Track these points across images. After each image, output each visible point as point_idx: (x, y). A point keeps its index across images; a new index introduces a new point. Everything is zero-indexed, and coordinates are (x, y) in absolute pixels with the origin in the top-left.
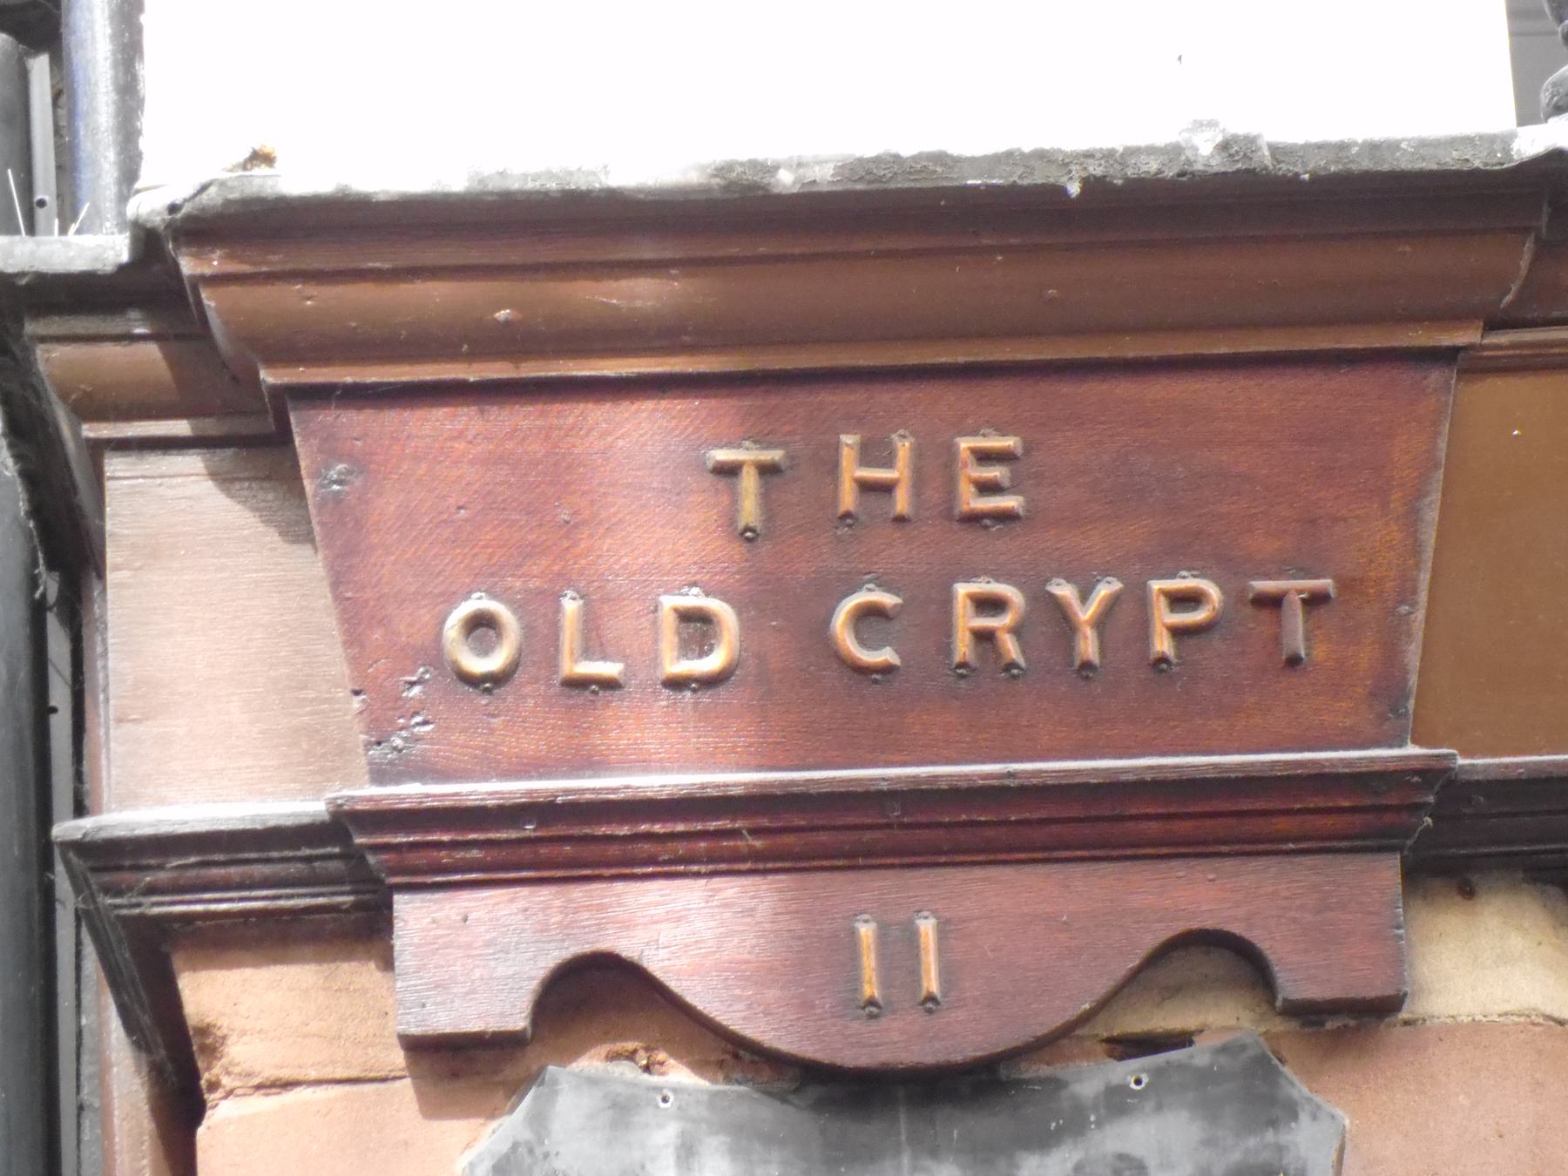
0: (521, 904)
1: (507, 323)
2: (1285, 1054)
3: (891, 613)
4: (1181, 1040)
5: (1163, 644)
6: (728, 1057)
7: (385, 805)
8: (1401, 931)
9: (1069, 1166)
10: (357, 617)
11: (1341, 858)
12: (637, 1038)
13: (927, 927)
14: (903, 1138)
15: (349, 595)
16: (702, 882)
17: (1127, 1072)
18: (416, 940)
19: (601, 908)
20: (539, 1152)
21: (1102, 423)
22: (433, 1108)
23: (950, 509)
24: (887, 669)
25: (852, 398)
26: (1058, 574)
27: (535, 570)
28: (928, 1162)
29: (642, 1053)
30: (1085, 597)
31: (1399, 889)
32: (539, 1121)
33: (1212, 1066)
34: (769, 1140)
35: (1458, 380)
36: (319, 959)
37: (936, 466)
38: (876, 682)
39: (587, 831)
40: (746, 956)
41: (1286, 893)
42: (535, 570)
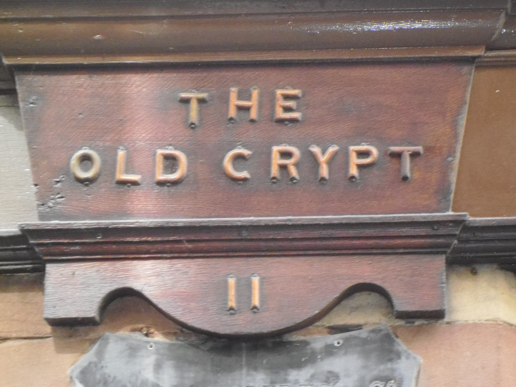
0: (96, 269)
1: (99, 40)
2: (398, 334)
3: (247, 157)
4: (359, 327)
5: (354, 171)
6: (178, 331)
7: (41, 227)
8: (444, 285)
9: (309, 375)
10: (37, 157)
11: (421, 256)
12: (143, 323)
13: (256, 281)
14: (244, 363)
15: (35, 147)
16: (169, 261)
17: (336, 339)
18: (54, 282)
19: (127, 271)
20: (99, 366)
21: (334, 85)
22: (60, 349)
23: (272, 117)
24: (245, 180)
25: (236, 73)
26: (314, 143)
27: (108, 138)
28: (254, 373)
29: (145, 329)
30: (324, 152)
31: (444, 268)
32: (100, 354)
33: (367, 337)
34: (191, 363)
35: (475, 71)
36: (20, 291)
37: (268, 101)
38: (240, 184)
39: (122, 239)
40: (183, 290)
41: (399, 269)
42: (108, 138)
